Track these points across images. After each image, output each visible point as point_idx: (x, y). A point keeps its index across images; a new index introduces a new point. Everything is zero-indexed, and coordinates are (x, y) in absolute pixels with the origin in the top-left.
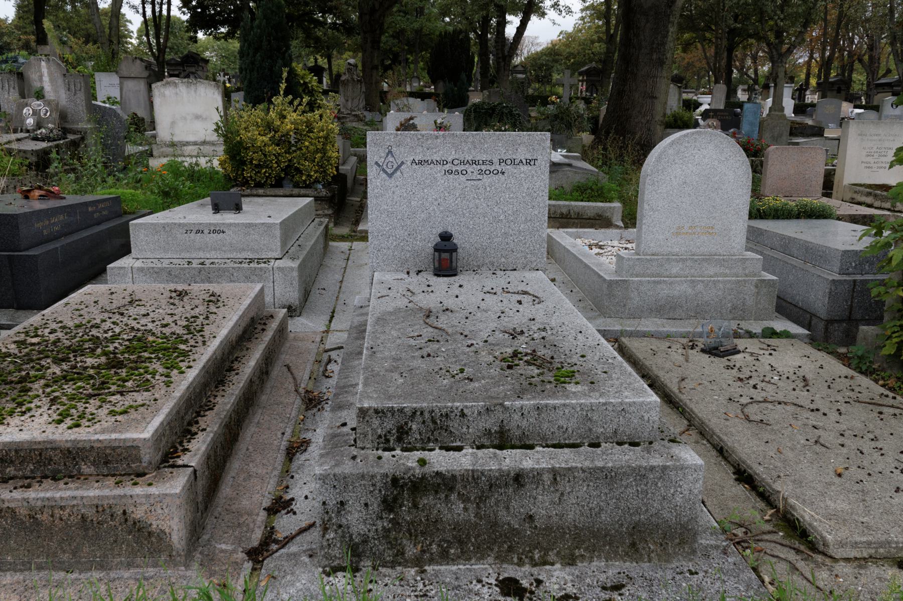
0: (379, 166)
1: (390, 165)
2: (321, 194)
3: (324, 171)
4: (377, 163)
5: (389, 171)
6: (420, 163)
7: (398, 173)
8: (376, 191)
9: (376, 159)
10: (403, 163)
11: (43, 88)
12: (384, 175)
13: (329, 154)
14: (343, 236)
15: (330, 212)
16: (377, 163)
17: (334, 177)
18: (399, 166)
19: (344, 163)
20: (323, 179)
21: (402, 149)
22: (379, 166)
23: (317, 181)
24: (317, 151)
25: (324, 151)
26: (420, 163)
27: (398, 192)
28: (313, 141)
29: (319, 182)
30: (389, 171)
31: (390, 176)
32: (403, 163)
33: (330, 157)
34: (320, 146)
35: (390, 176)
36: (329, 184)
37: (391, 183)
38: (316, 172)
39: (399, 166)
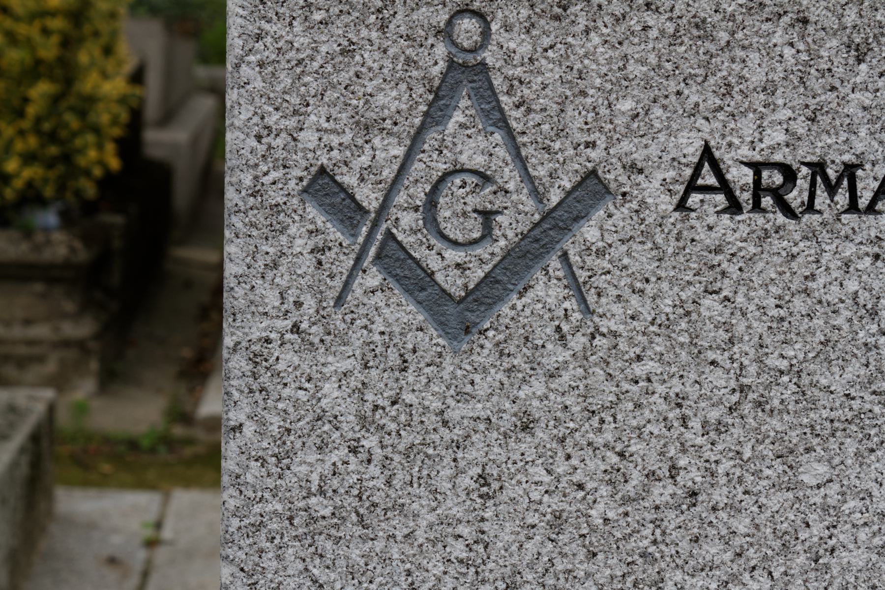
0: (346, 209)
1: (457, 208)
2: (47, 255)
3: (67, 158)
4: (323, 185)
5: (453, 269)
6: (774, 188)
7: (546, 290)
8: (308, 465)
9: (317, 139)
10: (592, 187)
11: (844, 163)
12: (401, 312)
13: (89, 83)
14: (133, 445)
15: (82, 329)
16: (323, 185)
17: (108, 182)
18: (552, 227)
19: (167, 118)
20: (61, 188)
21: (595, 51)
22: (346, 209)
23: (32, 197)
24: (35, 70)
25: (65, 72)
26: (774, 188)
27: (530, 484)
28: (22, 29)
29: (41, 202)
30: (453, 269)
31: (461, 315)
32: (592, 187)
33: (91, 100)
34: (49, 50)
35: (461, 315)
36: (89, 208)
37: (466, 385)
38: (29, 158)
39: (552, 227)
